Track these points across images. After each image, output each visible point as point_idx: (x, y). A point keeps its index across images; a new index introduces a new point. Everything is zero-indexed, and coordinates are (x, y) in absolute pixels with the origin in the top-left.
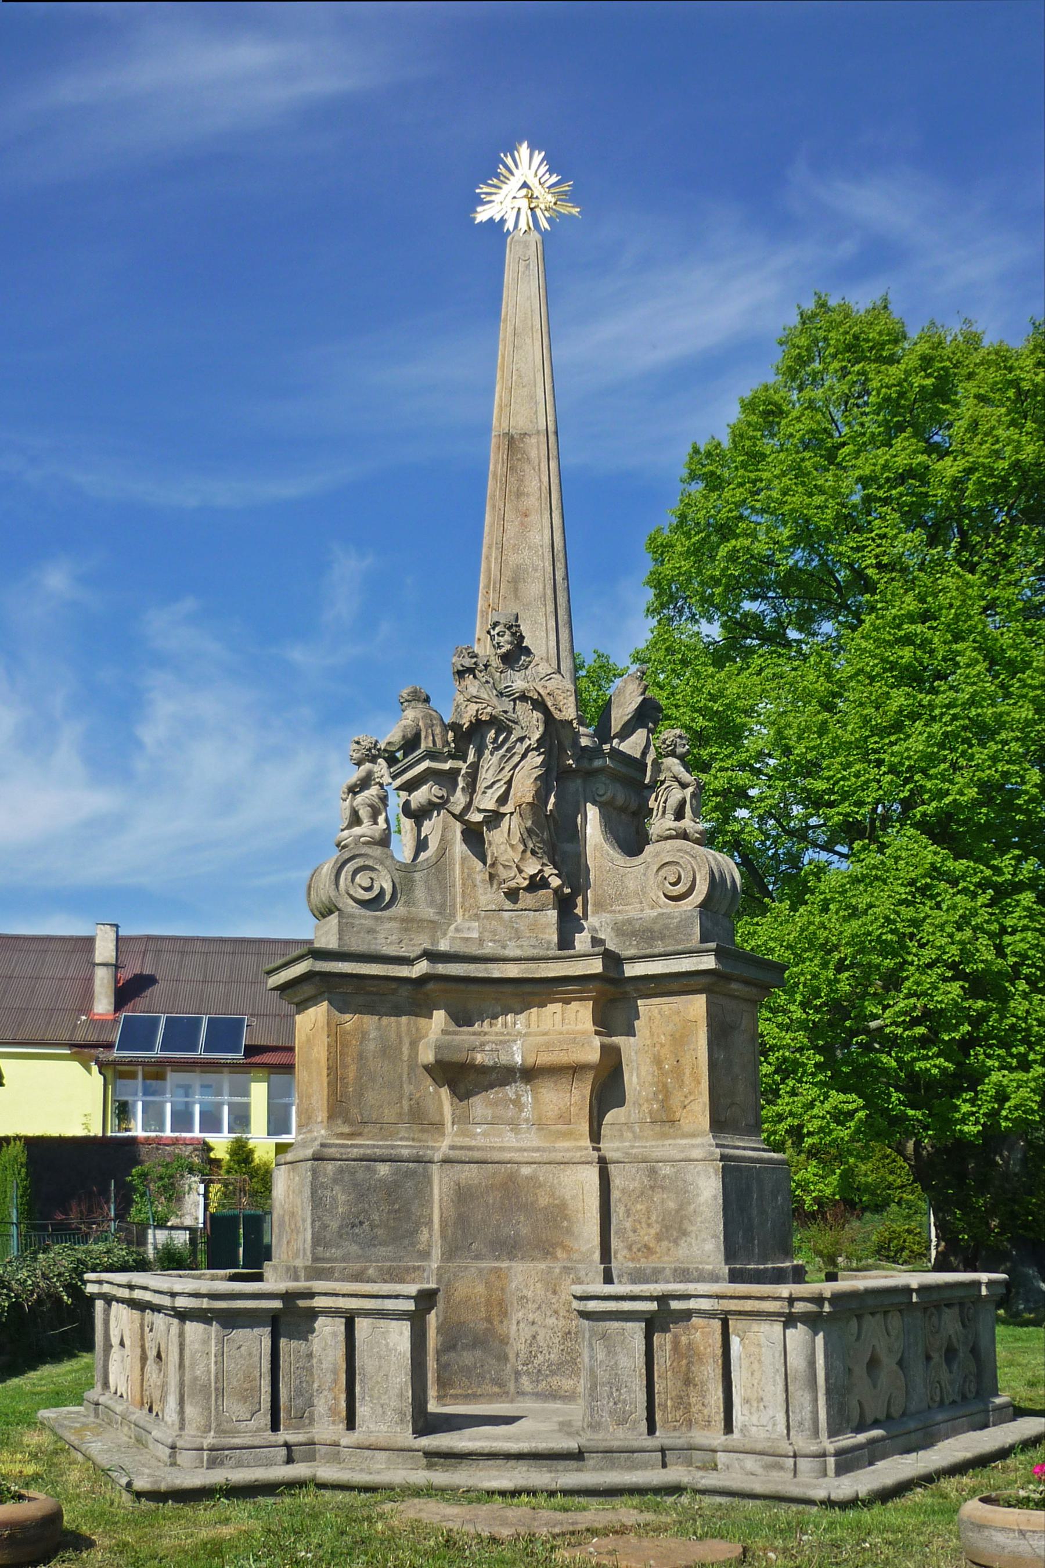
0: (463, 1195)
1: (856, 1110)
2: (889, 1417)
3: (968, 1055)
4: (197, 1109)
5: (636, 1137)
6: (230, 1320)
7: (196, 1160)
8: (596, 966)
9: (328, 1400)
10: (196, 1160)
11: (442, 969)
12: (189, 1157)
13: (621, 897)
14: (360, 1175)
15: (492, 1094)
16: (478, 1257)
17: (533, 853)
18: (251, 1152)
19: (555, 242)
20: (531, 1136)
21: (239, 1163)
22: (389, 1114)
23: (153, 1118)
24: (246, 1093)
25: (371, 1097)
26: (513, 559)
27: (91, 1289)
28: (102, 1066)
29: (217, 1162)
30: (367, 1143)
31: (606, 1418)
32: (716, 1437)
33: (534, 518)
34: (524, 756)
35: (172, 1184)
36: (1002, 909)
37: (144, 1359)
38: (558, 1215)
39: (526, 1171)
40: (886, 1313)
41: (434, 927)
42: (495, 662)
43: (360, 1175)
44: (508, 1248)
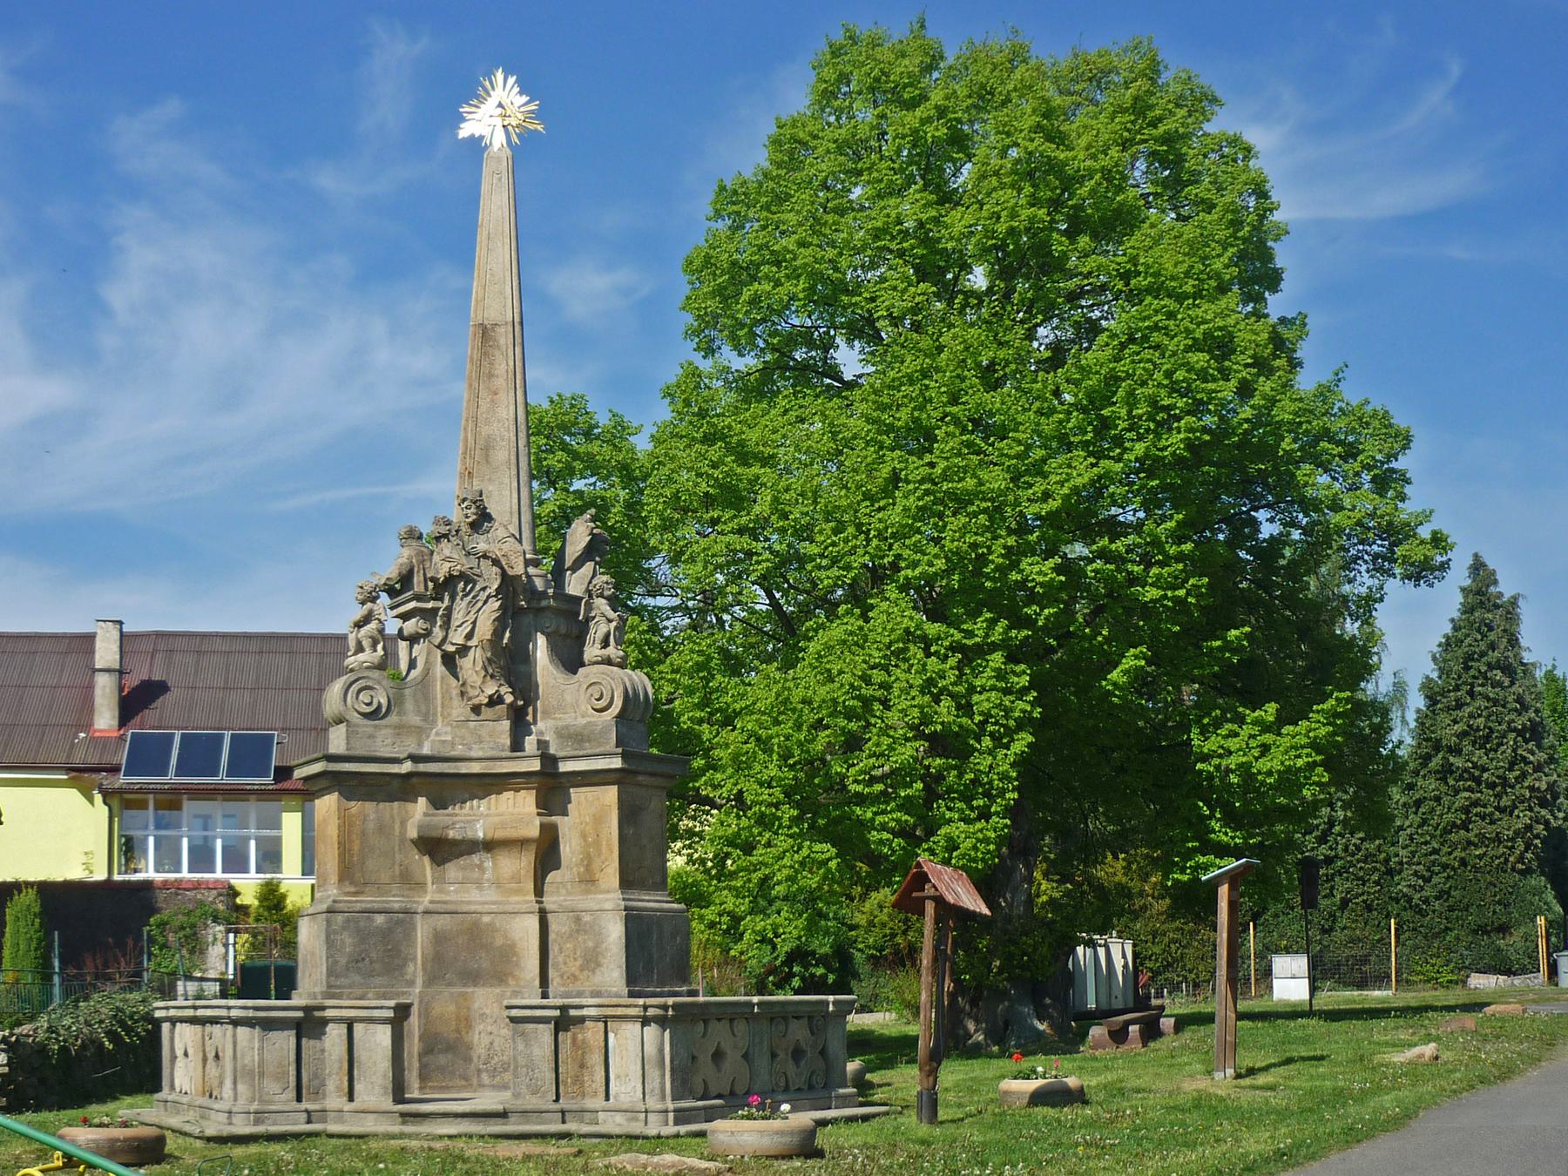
0: (439, 938)
1: (830, 859)
2: (732, 1093)
3: (931, 809)
4: (219, 844)
5: (569, 893)
6: (268, 1025)
7: (221, 907)
8: (535, 765)
9: (335, 1082)
10: (221, 907)
11: (422, 767)
12: (213, 903)
13: (561, 708)
14: (362, 924)
15: (461, 861)
16: (449, 984)
17: (492, 676)
18: (283, 897)
19: (524, 147)
20: (492, 893)
21: (269, 909)
22: (384, 877)
23: (168, 857)
24: (277, 825)
25: (371, 864)
26: (485, 430)
27: (158, 1014)
28: (107, 795)
29: (243, 910)
30: (368, 900)
31: (524, 1090)
32: (598, 1102)
33: (502, 396)
34: (485, 602)
35: (195, 934)
36: (973, 670)
37: (205, 1060)
40: (732, 1020)
41: (420, 732)
42: (465, 528)
43: (362, 924)
44: (473, 977)
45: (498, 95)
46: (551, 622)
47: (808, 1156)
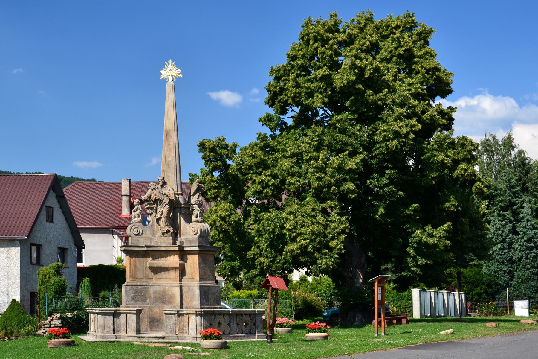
9: (123, 328)
11: (149, 249)
19: (177, 82)
26: (168, 159)
33: (172, 150)
38: (173, 296)
39: (167, 288)
40: (224, 315)
41: (151, 239)
45: (171, 67)
46: (183, 211)
47: (225, 348)
